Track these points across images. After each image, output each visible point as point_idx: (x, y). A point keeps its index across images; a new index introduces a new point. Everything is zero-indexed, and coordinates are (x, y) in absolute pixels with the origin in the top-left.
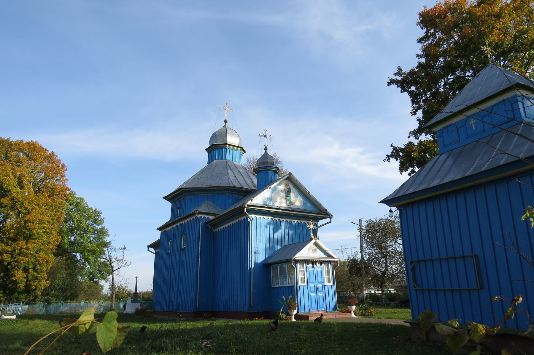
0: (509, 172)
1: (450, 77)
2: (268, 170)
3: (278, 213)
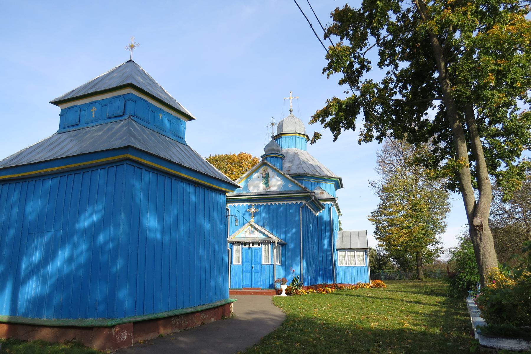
0: (52, 169)
1: (397, 70)
2: (267, 157)
3: (253, 199)
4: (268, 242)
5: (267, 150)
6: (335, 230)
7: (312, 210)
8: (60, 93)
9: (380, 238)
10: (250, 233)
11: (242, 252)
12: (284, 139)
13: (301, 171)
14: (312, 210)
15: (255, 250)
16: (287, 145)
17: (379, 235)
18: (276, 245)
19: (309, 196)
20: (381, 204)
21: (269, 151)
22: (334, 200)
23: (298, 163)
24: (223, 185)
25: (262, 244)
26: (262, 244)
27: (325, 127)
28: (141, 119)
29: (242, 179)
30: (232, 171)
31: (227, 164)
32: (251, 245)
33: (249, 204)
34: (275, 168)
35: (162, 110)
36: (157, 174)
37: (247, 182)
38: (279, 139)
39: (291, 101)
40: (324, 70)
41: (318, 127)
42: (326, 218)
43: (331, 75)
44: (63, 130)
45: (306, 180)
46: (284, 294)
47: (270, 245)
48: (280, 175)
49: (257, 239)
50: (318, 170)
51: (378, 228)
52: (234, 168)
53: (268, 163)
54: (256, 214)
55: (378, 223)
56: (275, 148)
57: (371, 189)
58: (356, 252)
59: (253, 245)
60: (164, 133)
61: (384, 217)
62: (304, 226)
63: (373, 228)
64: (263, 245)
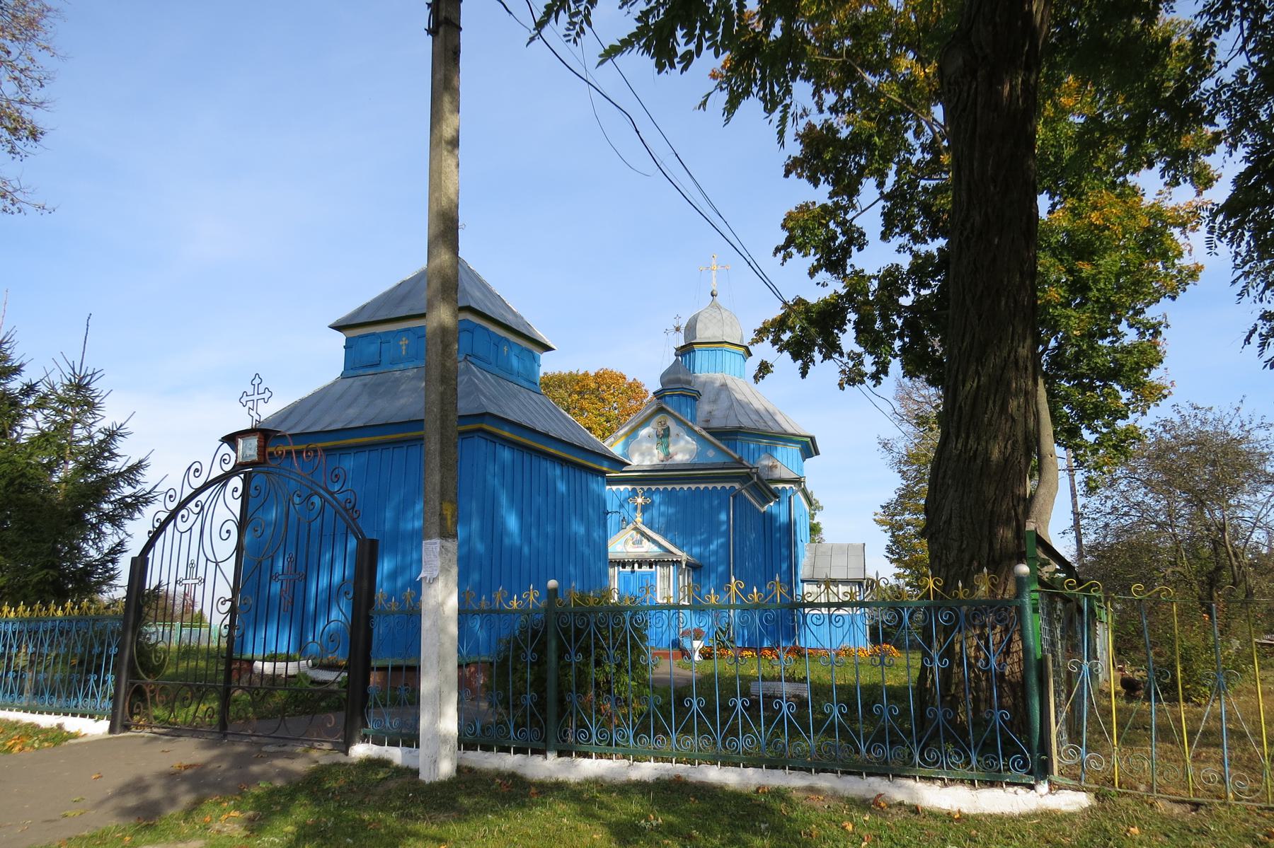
4: (668, 561)
5: (666, 379)
6: (799, 542)
7: (753, 501)
8: (343, 311)
9: (898, 561)
10: (633, 543)
11: (619, 580)
12: (698, 354)
13: (732, 423)
14: (753, 501)
15: (643, 575)
16: (705, 366)
17: (898, 553)
18: (684, 566)
19: (747, 473)
20: (903, 489)
21: (670, 382)
22: (798, 481)
23: (726, 404)
24: (606, 463)
25: (656, 566)
26: (656, 566)
27: (780, 350)
28: (480, 359)
29: (616, 439)
30: (582, 409)
31: (570, 395)
32: (636, 566)
33: (630, 487)
34: (682, 418)
35: (508, 340)
36: (495, 443)
37: (626, 445)
38: (689, 353)
39: (714, 273)
40: (777, 250)
41: (766, 350)
42: (783, 518)
43: (788, 260)
44: (352, 373)
45: (743, 440)
46: (697, 657)
47: (671, 567)
48: (691, 432)
49: (647, 556)
50: (767, 418)
51: (896, 540)
52: (586, 404)
53: (669, 409)
54: (645, 508)
55: (895, 528)
56: (681, 377)
57: (882, 456)
58: (840, 586)
59: (640, 567)
60: (511, 378)
61: (907, 516)
62: (738, 533)
63: (886, 539)
64: (658, 567)
